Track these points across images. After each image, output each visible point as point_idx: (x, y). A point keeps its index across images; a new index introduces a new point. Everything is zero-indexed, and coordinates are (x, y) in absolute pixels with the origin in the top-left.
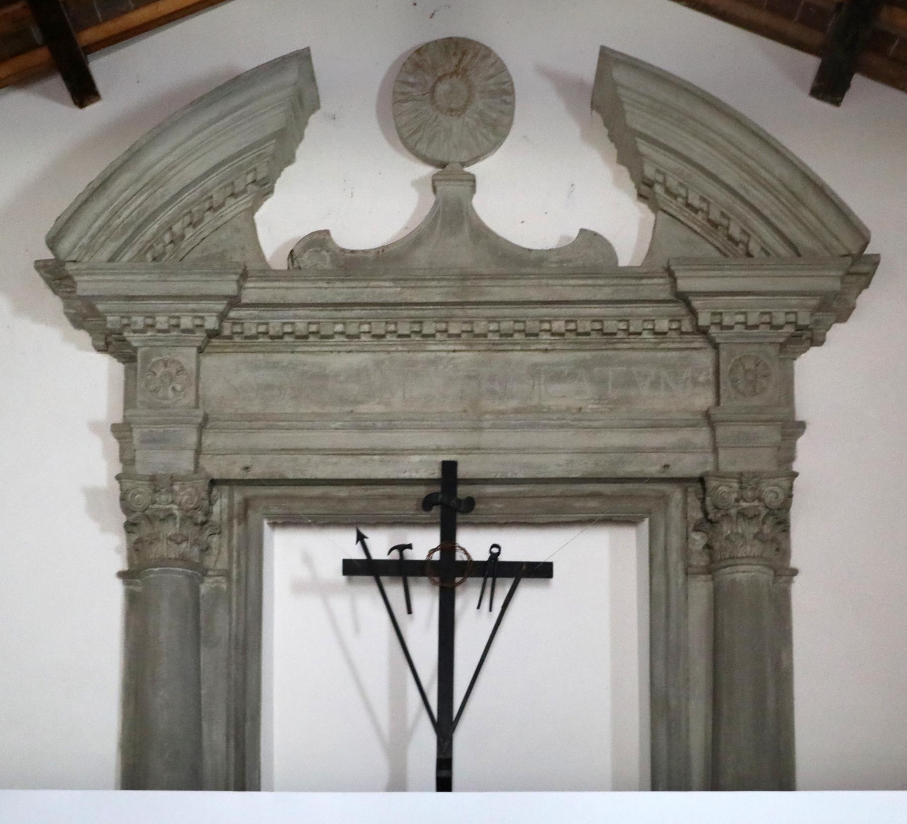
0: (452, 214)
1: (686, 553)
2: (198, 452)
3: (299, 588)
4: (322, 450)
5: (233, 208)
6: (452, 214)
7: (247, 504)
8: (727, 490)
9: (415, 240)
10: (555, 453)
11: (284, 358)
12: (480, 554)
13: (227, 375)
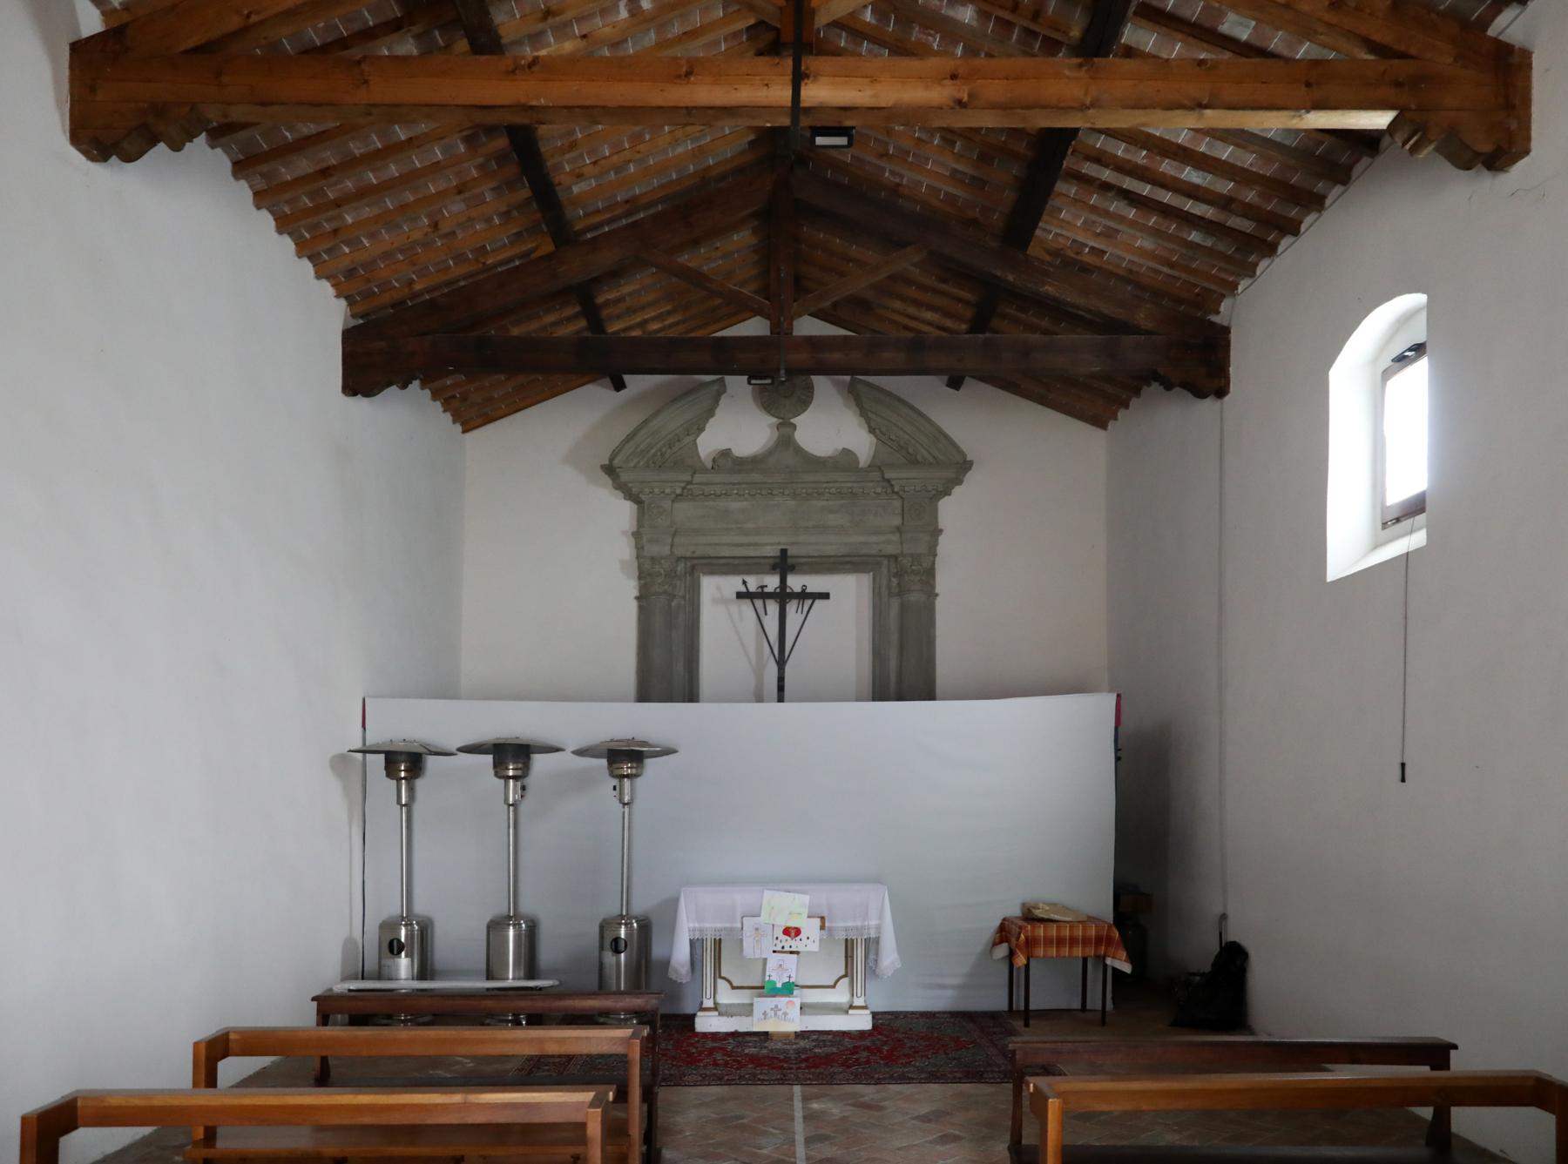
0: (786, 441)
1: (889, 587)
2: (672, 545)
3: (715, 601)
4: (728, 544)
5: (688, 439)
6: (786, 441)
7: (693, 568)
8: (906, 561)
9: (770, 453)
10: (831, 545)
11: (711, 503)
12: (797, 589)
13: (685, 512)
